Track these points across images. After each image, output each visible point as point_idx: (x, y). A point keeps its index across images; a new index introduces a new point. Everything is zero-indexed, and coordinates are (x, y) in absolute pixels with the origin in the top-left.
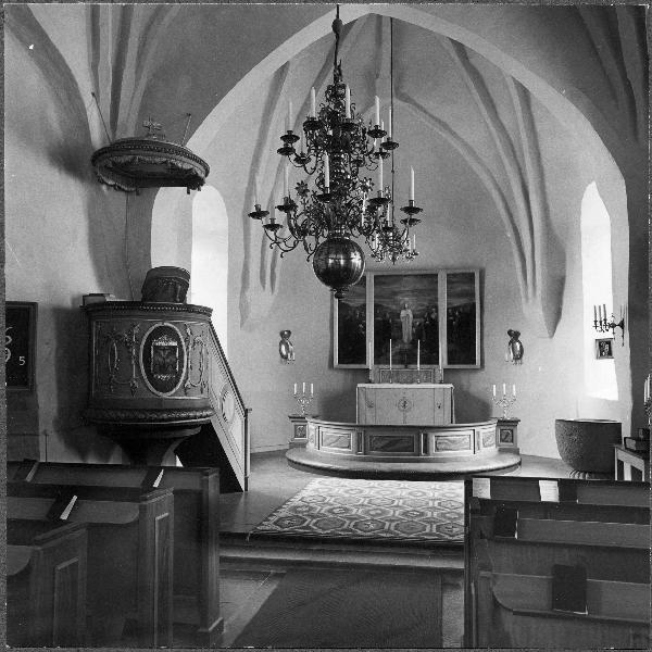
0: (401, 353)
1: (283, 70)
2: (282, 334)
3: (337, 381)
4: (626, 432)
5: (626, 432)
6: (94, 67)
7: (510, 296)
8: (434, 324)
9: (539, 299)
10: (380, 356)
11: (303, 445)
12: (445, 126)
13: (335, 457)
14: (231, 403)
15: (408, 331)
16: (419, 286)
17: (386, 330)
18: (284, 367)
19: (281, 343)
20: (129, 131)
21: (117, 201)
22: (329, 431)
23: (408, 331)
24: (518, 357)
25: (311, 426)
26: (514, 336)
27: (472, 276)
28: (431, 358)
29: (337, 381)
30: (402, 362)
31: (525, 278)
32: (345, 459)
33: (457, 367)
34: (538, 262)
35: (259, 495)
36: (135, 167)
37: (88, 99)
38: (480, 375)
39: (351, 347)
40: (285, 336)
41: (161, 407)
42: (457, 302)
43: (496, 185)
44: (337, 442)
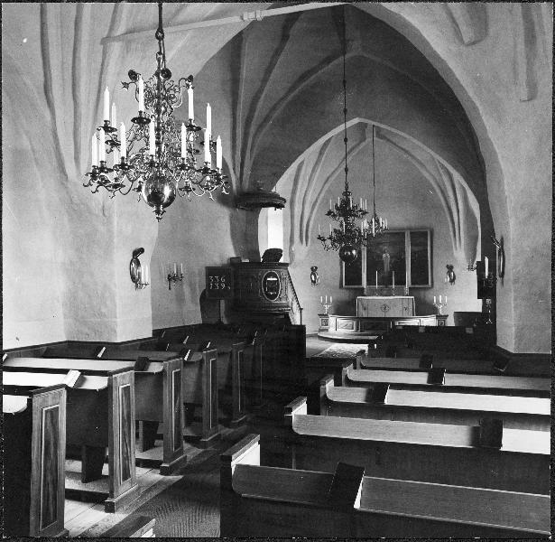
0: (383, 278)
1: (329, 140)
2: (312, 269)
3: (344, 295)
4: (366, 352)
5: (366, 352)
6: (233, 157)
7: (449, 248)
8: (403, 261)
9: (463, 247)
10: (370, 281)
11: (327, 330)
12: (406, 152)
13: (345, 334)
14: (295, 306)
15: (387, 267)
16: (393, 240)
17: (374, 264)
18: (314, 288)
19: (312, 274)
20: (246, 185)
21: (241, 214)
22: (342, 321)
23: (387, 267)
24: (452, 281)
25: (332, 320)
26: (450, 268)
27: (426, 234)
28: (401, 282)
29: (344, 295)
30: (383, 284)
31: (455, 236)
32: (356, 335)
33: (417, 286)
34: (462, 221)
35: (310, 349)
36: (249, 201)
37: (232, 171)
38: (431, 292)
39: (352, 277)
40: (314, 270)
41: (271, 306)
42: (416, 249)
43: (436, 182)
44: (346, 327)
